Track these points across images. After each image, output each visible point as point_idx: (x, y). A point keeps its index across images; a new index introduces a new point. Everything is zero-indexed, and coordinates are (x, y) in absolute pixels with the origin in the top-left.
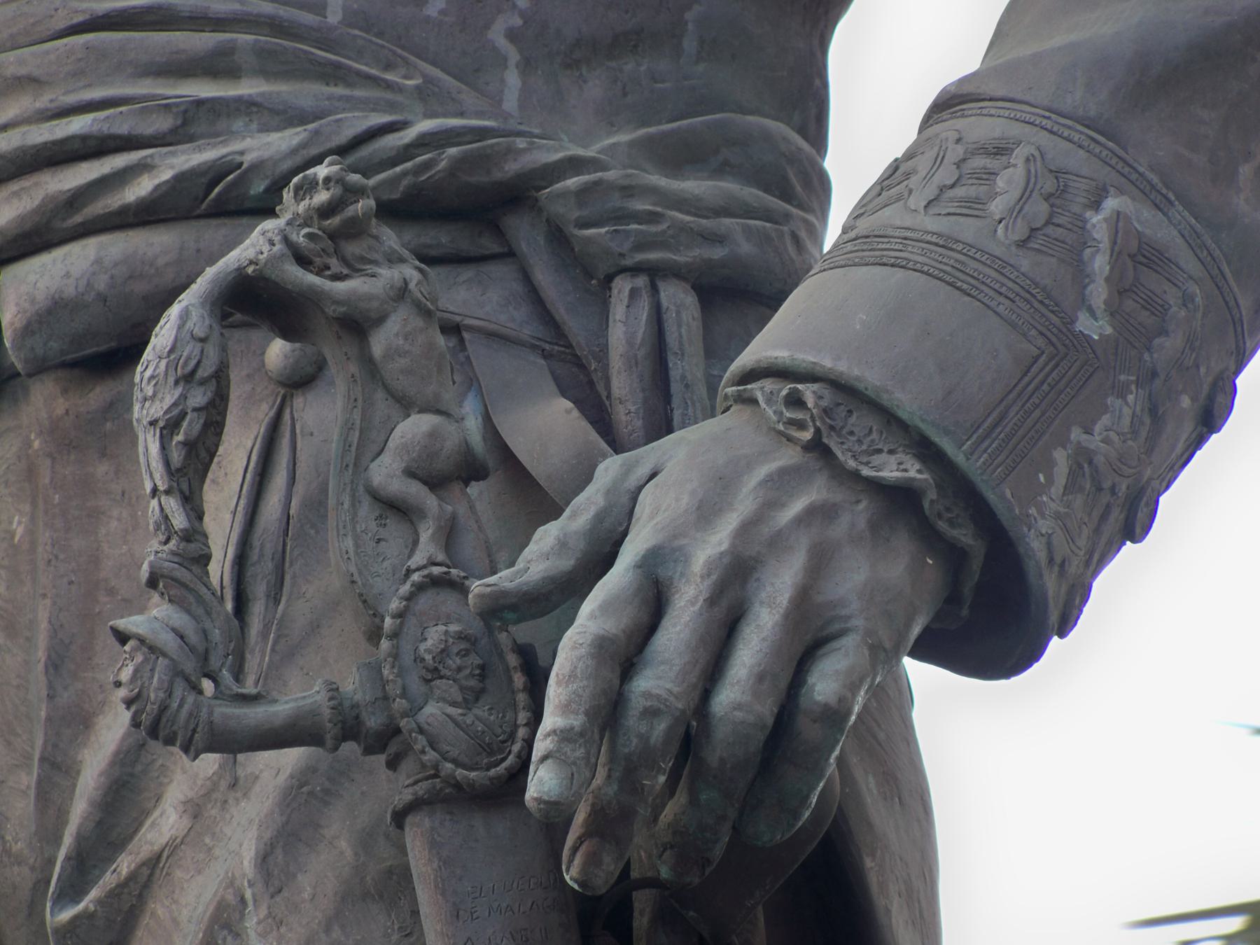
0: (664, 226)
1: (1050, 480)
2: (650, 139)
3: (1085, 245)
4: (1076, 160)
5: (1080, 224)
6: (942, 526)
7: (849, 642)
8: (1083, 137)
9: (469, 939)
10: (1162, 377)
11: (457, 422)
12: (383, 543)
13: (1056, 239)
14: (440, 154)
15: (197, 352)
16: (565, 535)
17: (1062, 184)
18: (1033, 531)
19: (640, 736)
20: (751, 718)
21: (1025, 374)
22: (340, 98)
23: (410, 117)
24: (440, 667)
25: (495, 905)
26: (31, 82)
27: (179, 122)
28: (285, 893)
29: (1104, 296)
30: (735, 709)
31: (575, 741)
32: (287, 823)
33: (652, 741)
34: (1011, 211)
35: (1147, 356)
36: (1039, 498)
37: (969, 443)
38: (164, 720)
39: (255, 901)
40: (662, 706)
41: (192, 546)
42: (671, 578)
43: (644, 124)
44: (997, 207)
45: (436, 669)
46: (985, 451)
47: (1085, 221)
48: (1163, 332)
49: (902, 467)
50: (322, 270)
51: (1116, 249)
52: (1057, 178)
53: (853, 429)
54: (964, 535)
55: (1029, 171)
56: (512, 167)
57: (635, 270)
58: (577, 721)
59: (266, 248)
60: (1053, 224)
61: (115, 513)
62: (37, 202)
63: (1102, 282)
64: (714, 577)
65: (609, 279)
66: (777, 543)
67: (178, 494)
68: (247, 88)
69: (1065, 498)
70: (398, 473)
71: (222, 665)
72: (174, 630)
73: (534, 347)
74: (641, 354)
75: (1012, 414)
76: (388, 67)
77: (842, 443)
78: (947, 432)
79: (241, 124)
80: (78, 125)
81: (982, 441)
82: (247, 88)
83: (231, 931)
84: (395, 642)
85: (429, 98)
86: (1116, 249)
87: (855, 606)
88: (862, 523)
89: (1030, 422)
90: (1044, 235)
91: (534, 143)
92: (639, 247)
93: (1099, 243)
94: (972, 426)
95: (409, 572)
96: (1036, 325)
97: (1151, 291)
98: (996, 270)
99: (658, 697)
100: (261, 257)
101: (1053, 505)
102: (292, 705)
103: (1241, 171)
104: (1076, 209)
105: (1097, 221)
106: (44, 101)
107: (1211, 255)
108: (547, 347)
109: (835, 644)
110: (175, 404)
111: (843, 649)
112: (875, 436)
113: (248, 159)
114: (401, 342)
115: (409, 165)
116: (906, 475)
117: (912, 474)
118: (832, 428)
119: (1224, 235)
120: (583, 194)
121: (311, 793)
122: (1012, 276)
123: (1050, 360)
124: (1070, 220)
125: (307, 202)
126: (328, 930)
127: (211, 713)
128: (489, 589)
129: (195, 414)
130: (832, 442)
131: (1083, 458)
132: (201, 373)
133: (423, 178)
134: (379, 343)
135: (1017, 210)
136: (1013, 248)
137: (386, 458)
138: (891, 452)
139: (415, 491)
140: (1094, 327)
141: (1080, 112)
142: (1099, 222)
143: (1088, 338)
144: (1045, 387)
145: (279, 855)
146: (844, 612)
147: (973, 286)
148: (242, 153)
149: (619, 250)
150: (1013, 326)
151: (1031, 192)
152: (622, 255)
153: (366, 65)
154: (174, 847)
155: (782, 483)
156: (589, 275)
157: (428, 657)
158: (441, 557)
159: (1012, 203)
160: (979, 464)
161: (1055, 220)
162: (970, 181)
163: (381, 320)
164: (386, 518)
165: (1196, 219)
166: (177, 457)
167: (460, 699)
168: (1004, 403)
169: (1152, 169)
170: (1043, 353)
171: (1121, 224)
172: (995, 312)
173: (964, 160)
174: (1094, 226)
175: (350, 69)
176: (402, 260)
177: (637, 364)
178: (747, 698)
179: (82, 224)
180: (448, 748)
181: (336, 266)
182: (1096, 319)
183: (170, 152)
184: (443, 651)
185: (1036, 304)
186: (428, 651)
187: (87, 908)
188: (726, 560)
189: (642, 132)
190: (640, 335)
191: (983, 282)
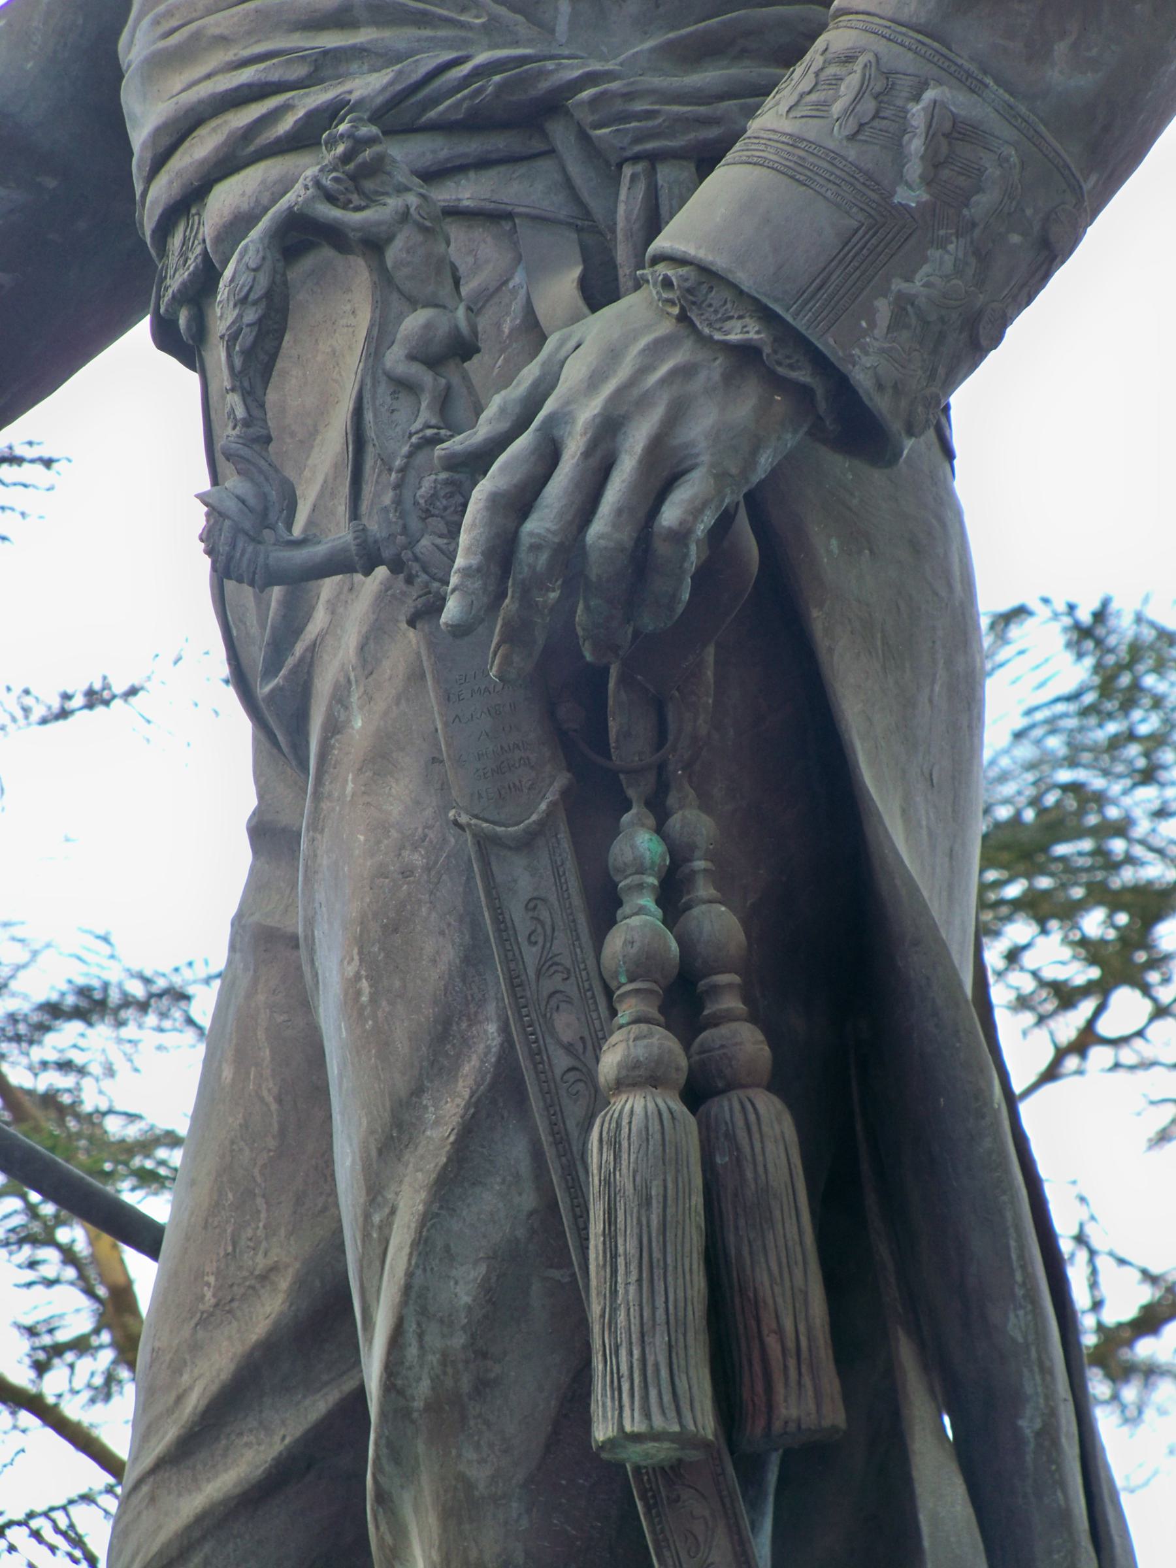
0: (660, 120)
1: (872, 324)
2: (671, 44)
3: (905, 132)
4: (905, 61)
5: (902, 114)
6: (781, 370)
7: (696, 475)
8: (912, 41)
9: (457, 716)
10: (982, 226)
11: (451, 311)
12: (396, 413)
13: (881, 130)
14: (488, 82)
15: (250, 280)
16: (505, 403)
17: (890, 83)
18: (857, 367)
19: (529, 566)
20: (612, 544)
21: (847, 244)
22: (428, 39)
23: (471, 51)
24: (431, 509)
25: (476, 688)
26: (223, 40)
27: (312, 69)
28: (374, 676)
29: (919, 171)
30: (599, 538)
31: (474, 576)
32: (377, 620)
33: (538, 568)
34: (846, 111)
35: (965, 212)
36: (862, 340)
37: (795, 306)
38: (232, 566)
39: (356, 681)
40: (542, 542)
41: (251, 430)
42: (562, 437)
43: (673, 28)
44: (837, 108)
45: (428, 510)
46: (810, 310)
47: (907, 112)
48: (979, 190)
49: (745, 330)
50: (348, 204)
51: (931, 133)
52: (887, 78)
53: (712, 302)
54: (803, 376)
55: (864, 76)
56: (544, 85)
57: (636, 158)
58: (475, 561)
59: (302, 192)
60: (879, 117)
61: (294, 373)
62: (225, 136)
63: (917, 160)
64: (589, 435)
65: (620, 166)
66: (644, 402)
67: (240, 392)
68: (363, 36)
69: (889, 336)
70: (403, 358)
71: (278, 519)
72: (238, 497)
73: (569, 224)
74: (636, 227)
75: (834, 277)
76: (464, 9)
77: (702, 314)
78: (776, 300)
79: (356, 66)
80: (246, 75)
81: (806, 304)
82: (363, 36)
83: (343, 705)
84: (398, 491)
85: (493, 31)
86: (931, 133)
87: (702, 444)
88: (716, 376)
89: (849, 283)
90: (871, 128)
91: (560, 64)
92: (637, 140)
93: (916, 128)
94: (798, 292)
95: (411, 435)
96: (858, 203)
97: (966, 159)
98: (829, 162)
99: (538, 535)
100: (300, 199)
101: (876, 344)
102: (329, 545)
103: (1056, 47)
104: (900, 102)
105: (917, 113)
106: (230, 55)
107: (1026, 121)
108: (579, 223)
109: (687, 477)
110: (233, 323)
111: (690, 482)
112: (729, 305)
113: (354, 97)
114: (405, 255)
115: (466, 92)
116: (746, 336)
117: (752, 335)
118: (694, 303)
119: (1038, 103)
120: (594, 101)
121: (393, 596)
122: (841, 166)
123: (870, 229)
124: (894, 112)
125: (333, 153)
126: (398, 704)
127: (267, 557)
128: (443, 452)
129: (249, 329)
130: (693, 316)
131: (903, 304)
132: (253, 297)
133: (477, 101)
134: (393, 254)
135: (849, 111)
136: (845, 142)
137: (395, 348)
138: (740, 317)
139: (416, 370)
140: (910, 196)
141: (914, 20)
142: (917, 111)
143: (906, 207)
144: (865, 251)
145: (372, 645)
146: (696, 451)
147: (808, 177)
148: (350, 92)
149: (621, 145)
150: (838, 206)
151: (864, 93)
152: (623, 149)
153: (448, 9)
154: (322, 636)
155: (658, 349)
156: (608, 164)
157: (422, 501)
158: (433, 422)
159: (848, 103)
160: (803, 322)
161: (882, 114)
162: (824, 87)
163: (390, 239)
164: (399, 392)
165: (1011, 94)
166: (238, 362)
167: (445, 531)
168: (827, 270)
169: (972, 59)
170: (863, 225)
171: (936, 110)
172: (825, 197)
173: (822, 69)
174: (913, 115)
175: (433, 14)
176: (408, 189)
177: (632, 236)
178: (608, 529)
179: (255, 152)
180: (436, 571)
181: (356, 199)
182: (913, 190)
183: (305, 94)
184: (433, 495)
185: (859, 186)
186: (422, 497)
187: (278, 683)
188: (598, 420)
189: (671, 35)
190: (636, 212)
191: (817, 173)
